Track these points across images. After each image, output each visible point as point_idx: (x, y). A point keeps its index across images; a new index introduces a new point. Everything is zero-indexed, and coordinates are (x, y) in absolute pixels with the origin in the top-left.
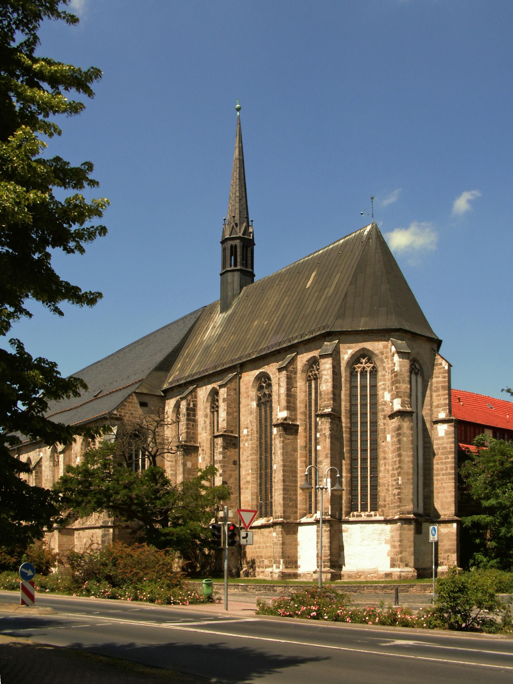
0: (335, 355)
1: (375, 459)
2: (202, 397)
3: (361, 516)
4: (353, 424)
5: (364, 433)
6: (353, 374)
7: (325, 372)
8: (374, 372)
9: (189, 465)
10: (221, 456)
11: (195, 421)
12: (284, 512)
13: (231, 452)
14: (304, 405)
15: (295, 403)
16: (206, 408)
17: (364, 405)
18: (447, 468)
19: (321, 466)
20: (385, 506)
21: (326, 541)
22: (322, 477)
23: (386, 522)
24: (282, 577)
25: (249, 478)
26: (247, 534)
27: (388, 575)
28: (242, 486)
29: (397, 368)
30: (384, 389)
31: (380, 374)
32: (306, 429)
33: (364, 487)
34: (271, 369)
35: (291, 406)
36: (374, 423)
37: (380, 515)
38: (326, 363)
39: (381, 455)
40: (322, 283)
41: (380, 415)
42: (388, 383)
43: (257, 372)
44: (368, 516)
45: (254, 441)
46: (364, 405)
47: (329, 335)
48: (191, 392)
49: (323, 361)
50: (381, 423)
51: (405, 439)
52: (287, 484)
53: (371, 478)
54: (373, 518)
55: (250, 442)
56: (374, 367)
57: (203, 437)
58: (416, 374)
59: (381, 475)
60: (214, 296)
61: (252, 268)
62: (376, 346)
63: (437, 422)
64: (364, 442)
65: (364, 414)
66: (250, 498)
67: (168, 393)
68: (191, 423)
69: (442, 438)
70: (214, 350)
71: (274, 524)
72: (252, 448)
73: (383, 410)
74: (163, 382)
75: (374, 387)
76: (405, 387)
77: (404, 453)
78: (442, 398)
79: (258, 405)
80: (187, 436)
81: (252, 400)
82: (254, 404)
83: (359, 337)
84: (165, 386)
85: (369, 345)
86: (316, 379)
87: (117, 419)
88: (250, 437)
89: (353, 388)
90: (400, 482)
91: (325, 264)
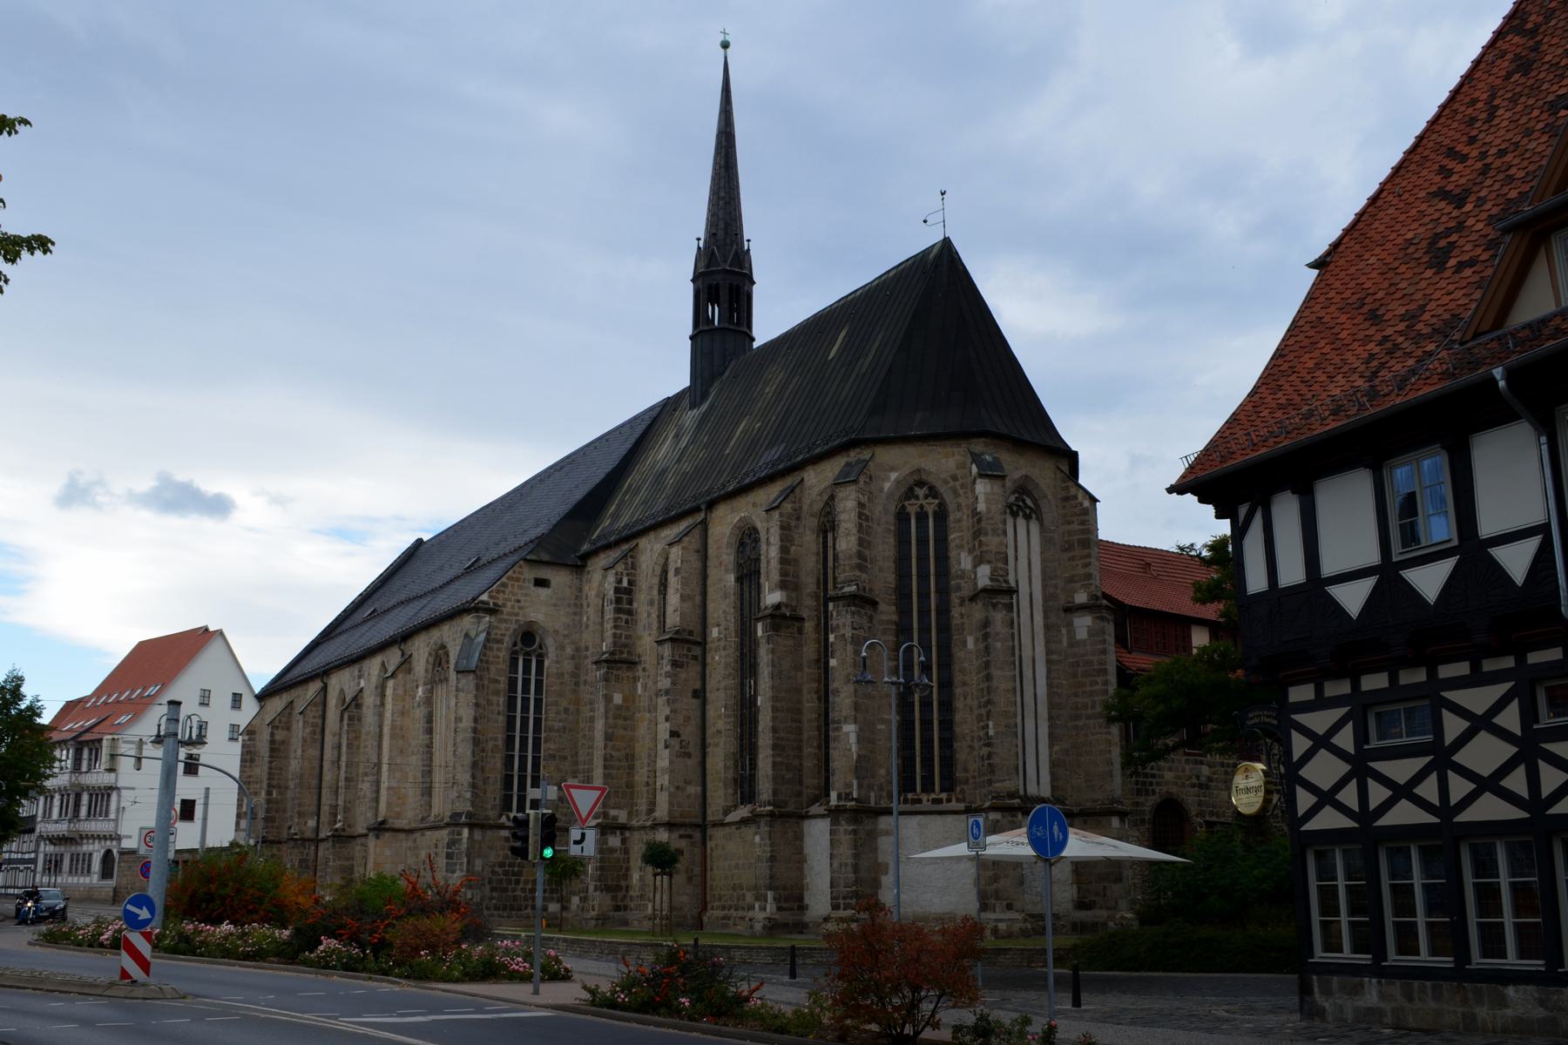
2: (644, 566)
3: (920, 801)
7: (843, 517)
8: (942, 515)
9: (618, 699)
10: (668, 681)
11: (630, 612)
12: (775, 793)
13: (690, 674)
14: (814, 580)
16: (651, 588)
18: (1094, 703)
19: (838, 700)
20: (966, 782)
21: (846, 851)
22: (838, 722)
23: (968, 811)
24: (771, 928)
25: (720, 725)
26: (583, 835)
28: (709, 740)
30: (960, 547)
32: (818, 625)
35: (787, 583)
36: (944, 610)
37: (958, 800)
38: (846, 499)
39: (958, 678)
41: (955, 598)
44: (935, 801)
45: (731, 651)
50: (956, 612)
51: (999, 645)
52: (782, 735)
53: (940, 722)
54: (944, 806)
55: (723, 653)
56: (940, 505)
57: (646, 642)
58: (1027, 518)
59: (958, 717)
66: (721, 765)
68: (624, 617)
69: (1084, 642)
70: (670, 480)
72: (727, 665)
73: (959, 588)
75: (942, 540)
77: (996, 673)
78: (1080, 563)
79: (739, 580)
80: (615, 643)
81: (727, 571)
82: (731, 578)
84: (585, 547)
86: (833, 529)
88: (722, 643)
90: (991, 733)
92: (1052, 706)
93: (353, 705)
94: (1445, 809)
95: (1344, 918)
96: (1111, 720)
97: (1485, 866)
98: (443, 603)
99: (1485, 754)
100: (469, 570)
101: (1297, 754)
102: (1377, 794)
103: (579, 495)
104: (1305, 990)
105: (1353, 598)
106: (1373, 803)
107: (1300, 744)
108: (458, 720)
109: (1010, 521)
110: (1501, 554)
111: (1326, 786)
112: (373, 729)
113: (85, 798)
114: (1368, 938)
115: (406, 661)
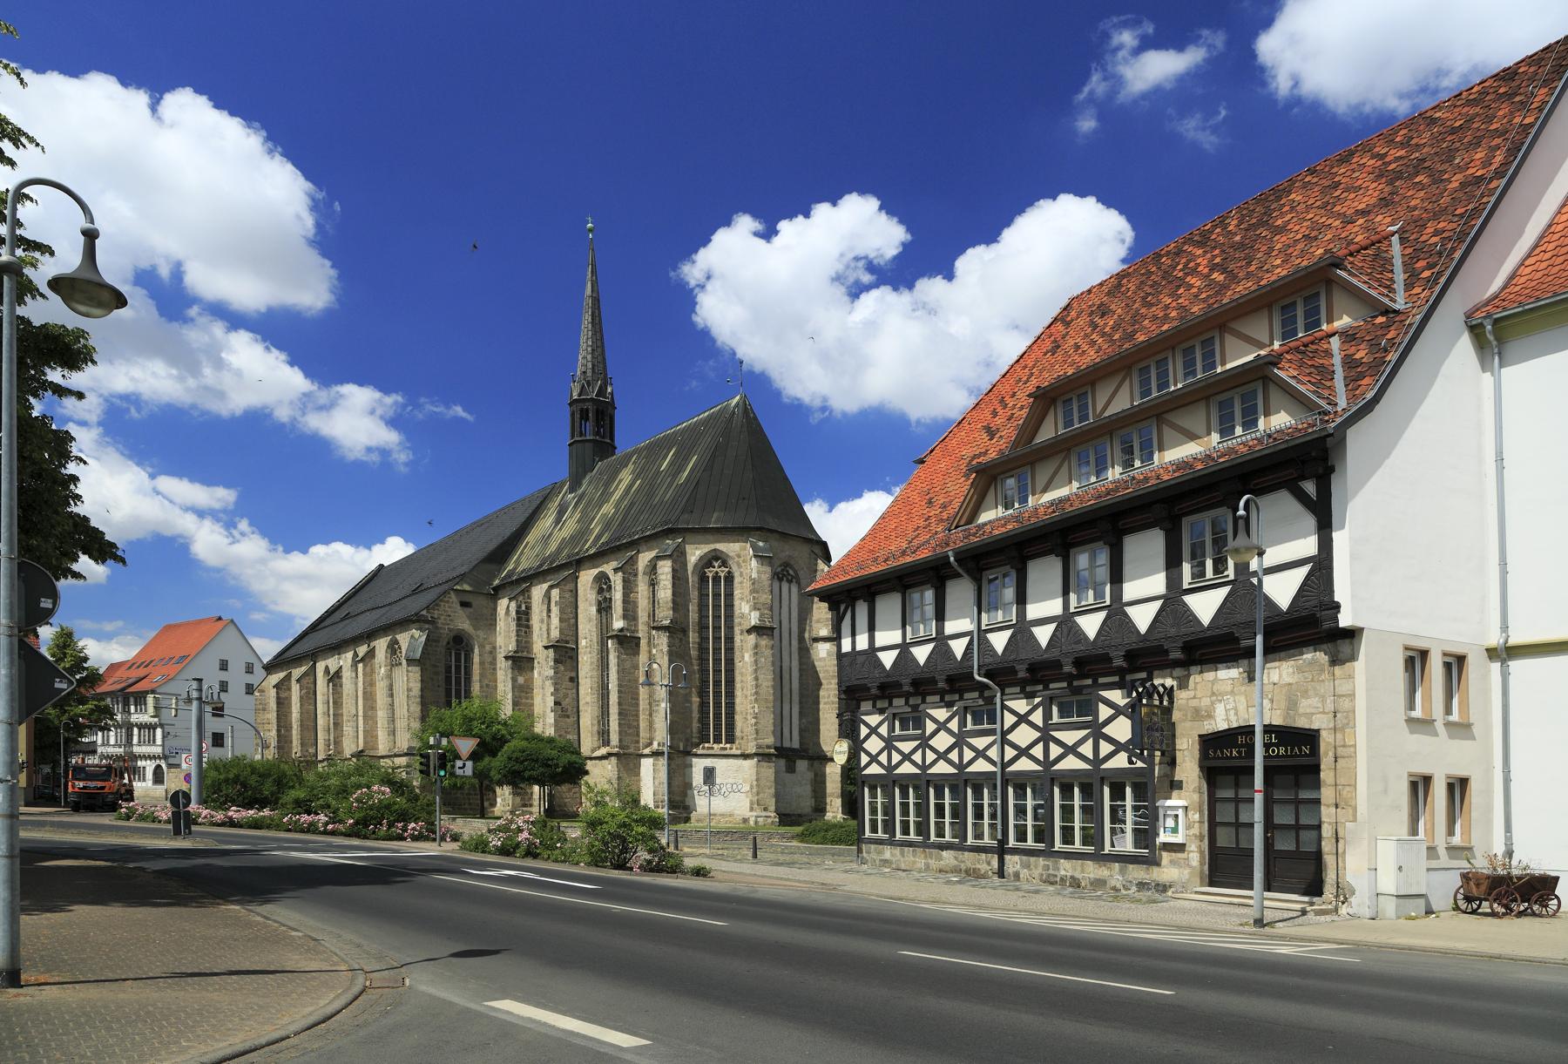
0: (678, 557)
1: (731, 682)
4: (704, 638)
5: (717, 650)
6: (703, 579)
8: (730, 578)
9: (521, 680)
11: (528, 627)
15: (635, 612)
17: (717, 617)
23: (745, 756)
25: (588, 699)
27: (745, 820)
29: (754, 575)
31: (737, 581)
33: (717, 716)
34: (608, 568)
36: (730, 639)
39: (738, 678)
40: (677, 466)
41: (737, 630)
42: (747, 592)
43: (595, 571)
46: (717, 617)
47: (670, 532)
48: (523, 592)
49: (660, 563)
50: (738, 638)
58: (790, 582)
59: (738, 701)
60: (561, 468)
61: (612, 438)
62: (730, 548)
63: (816, 640)
64: (717, 661)
65: (717, 628)
67: (496, 593)
71: (610, 755)
74: (495, 577)
75: (730, 596)
76: (765, 598)
77: (761, 677)
79: (599, 611)
82: (594, 609)
83: (710, 537)
85: (722, 547)
87: (427, 622)
89: (703, 596)
91: (685, 443)
92: (801, 696)
93: (335, 678)
94: (961, 766)
95: (947, 820)
96: (1352, 634)
97: (905, 795)
98: (397, 613)
99: (1024, 735)
100: (415, 592)
101: (1102, 719)
102: (1055, 751)
103: (492, 546)
104: (860, 851)
105: (888, 659)
106: (1052, 757)
107: (864, 731)
108: (409, 690)
109: (776, 584)
110: (1036, 631)
111: (942, 750)
112: (352, 692)
113: (136, 730)
114: (889, 826)
115: (371, 654)
